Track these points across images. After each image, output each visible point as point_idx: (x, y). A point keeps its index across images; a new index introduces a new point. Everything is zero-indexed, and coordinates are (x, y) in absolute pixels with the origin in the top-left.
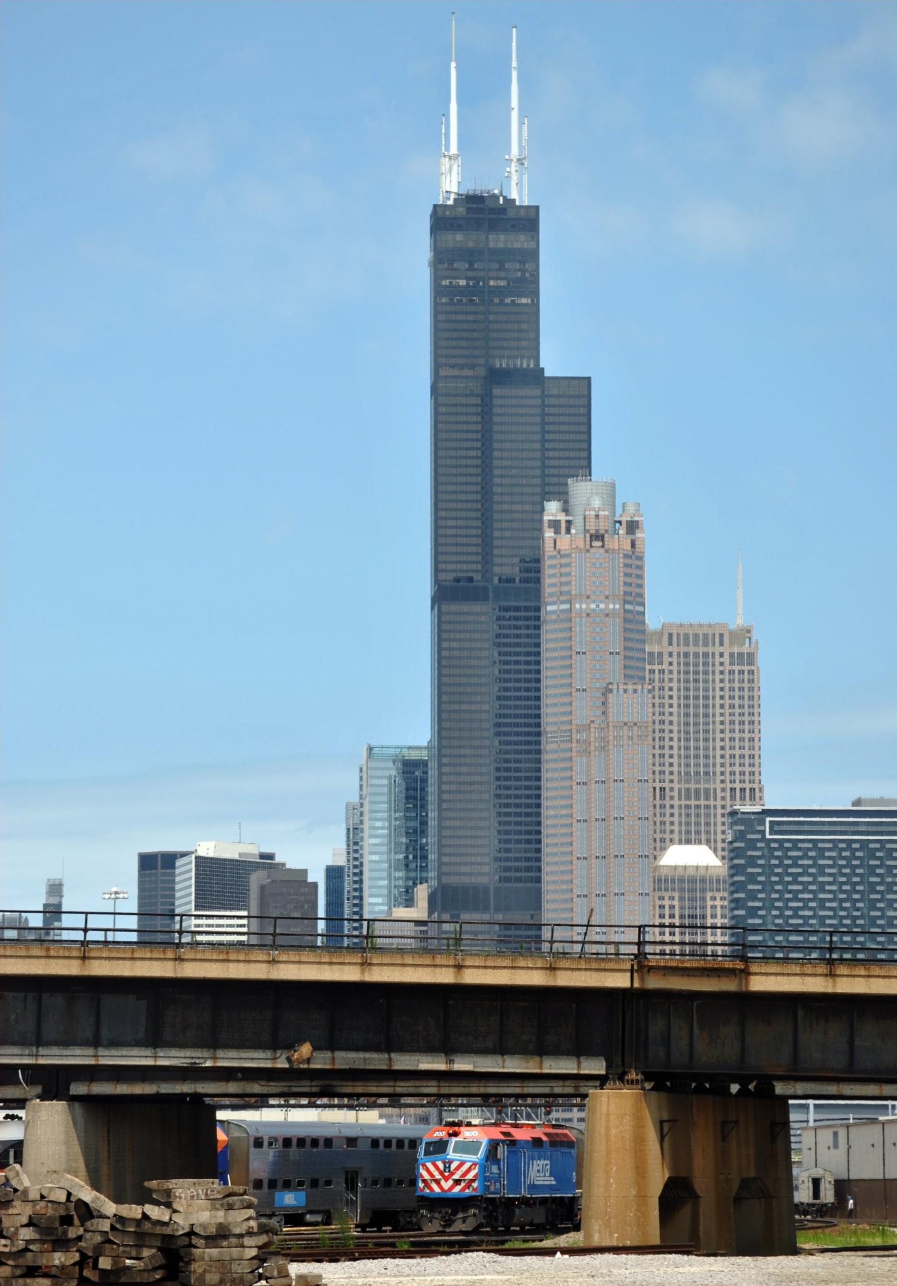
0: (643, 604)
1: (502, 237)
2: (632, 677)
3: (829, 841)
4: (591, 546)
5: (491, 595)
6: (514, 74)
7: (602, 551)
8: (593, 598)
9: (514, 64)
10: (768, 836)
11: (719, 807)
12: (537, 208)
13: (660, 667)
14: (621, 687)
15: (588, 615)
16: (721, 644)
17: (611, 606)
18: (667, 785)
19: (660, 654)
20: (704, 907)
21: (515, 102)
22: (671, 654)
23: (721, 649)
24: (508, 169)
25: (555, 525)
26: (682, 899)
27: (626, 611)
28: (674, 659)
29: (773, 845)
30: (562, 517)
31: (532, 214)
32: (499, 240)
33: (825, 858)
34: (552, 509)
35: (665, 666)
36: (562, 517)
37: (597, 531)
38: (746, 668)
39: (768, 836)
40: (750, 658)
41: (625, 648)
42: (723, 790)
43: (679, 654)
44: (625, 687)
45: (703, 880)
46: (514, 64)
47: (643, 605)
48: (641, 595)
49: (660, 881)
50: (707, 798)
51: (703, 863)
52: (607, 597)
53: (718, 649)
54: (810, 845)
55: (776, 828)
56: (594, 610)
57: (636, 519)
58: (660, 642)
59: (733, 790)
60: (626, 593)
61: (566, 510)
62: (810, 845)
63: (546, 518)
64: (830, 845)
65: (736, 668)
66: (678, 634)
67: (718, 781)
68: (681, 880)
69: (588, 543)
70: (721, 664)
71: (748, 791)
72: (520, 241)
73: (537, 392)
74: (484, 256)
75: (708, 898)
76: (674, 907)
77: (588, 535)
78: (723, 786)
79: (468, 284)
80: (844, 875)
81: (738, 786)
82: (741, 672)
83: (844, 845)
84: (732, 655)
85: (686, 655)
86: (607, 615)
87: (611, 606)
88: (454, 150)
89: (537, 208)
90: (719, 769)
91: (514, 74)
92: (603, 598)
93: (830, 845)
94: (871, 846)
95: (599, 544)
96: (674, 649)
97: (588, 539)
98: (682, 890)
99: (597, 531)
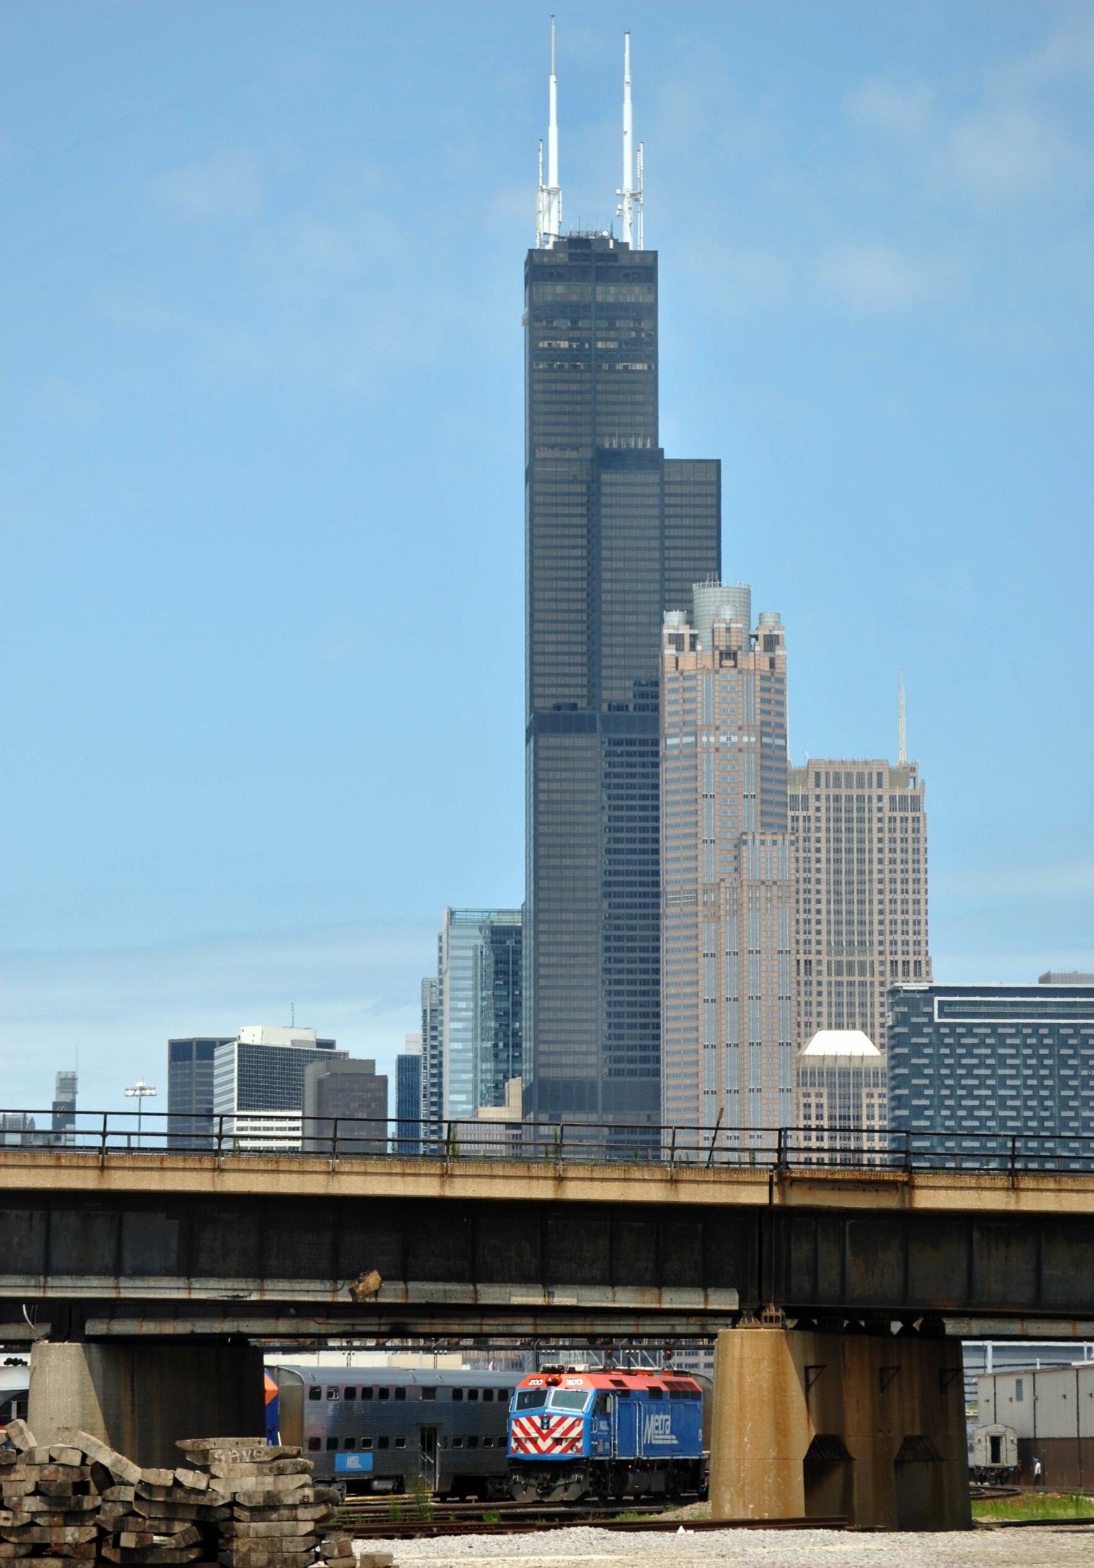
0: (784, 737)
1: (612, 290)
2: (771, 825)
3: (1011, 1025)
4: (721, 666)
5: (599, 725)
6: (627, 91)
7: (734, 671)
8: (723, 728)
9: (627, 78)
10: (937, 1020)
11: (877, 984)
12: (655, 254)
13: (805, 813)
14: (758, 837)
15: (717, 750)
16: (880, 785)
17: (745, 739)
18: (813, 957)
19: (805, 798)
20: (858, 1106)
21: (627, 125)
22: (818, 798)
23: (880, 792)
24: (620, 207)
25: (677, 640)
26: (831, 1096)
27: (763, 745)
28: (823, 804)
29: (943, 1030)
30: (686, 631)
31: (649, 261)
32: (608, 293)
33: (1005, 1046)
34: (674, 620)
35: (811, 812)
36: (686, 631)
37: (728, 647)
38: (910, 815)
39: (937, 1020)
40: (915, 802)
41: (763, 790)
42: (882, 963)
43: (828, 797)
44: (763, 838)
45: (857, 1074)
46: (627, 78)
47: (784, 737)
48: (782, 726)
49: (805, 1074)
50: (862, 973)
51: (857, 1052)
52: (740, 728)
53: (876, 792)
54: (988, 1031)
55: (947, 1010)
56: (725, 744)
57: (776, 632)
58: (804, 782)
59: (894, 963)
60: (763, 723)
61: (690, 622)
62: (988, 1031)
63: (666, 632)
64: (1013, 1031)
65: (898, 814)
66: (827, 774)
67: (876, 953)
68: (831, 1073)
69: (717, 662)
70: (880, 809)
71: (912, 965)
72: (634, 294)
73: (655, 478)
74: (590, 312)
75: (864, 1095)
76: (822, 1106)
77: (717, 653)
78: (881, 958)
79: (571, 346)
80: (1029, 1067)
81: (900, 958)
82: (904, 820)
83: (1029, 1031)
84: (892, 799)
85: (837, 798)
86: (740, 750)
87: (745, 739)
88: (553, 182)
89: (655, 254)
90: (876, 938)
91: (627, 91)
92: (735, 729)
93: (1013, 1031)
94: (1063, 1031)
95: (732, 663)
96: (822, 791)
97: (717, 657)
98: (832, 1085)
99: (728, 647)
